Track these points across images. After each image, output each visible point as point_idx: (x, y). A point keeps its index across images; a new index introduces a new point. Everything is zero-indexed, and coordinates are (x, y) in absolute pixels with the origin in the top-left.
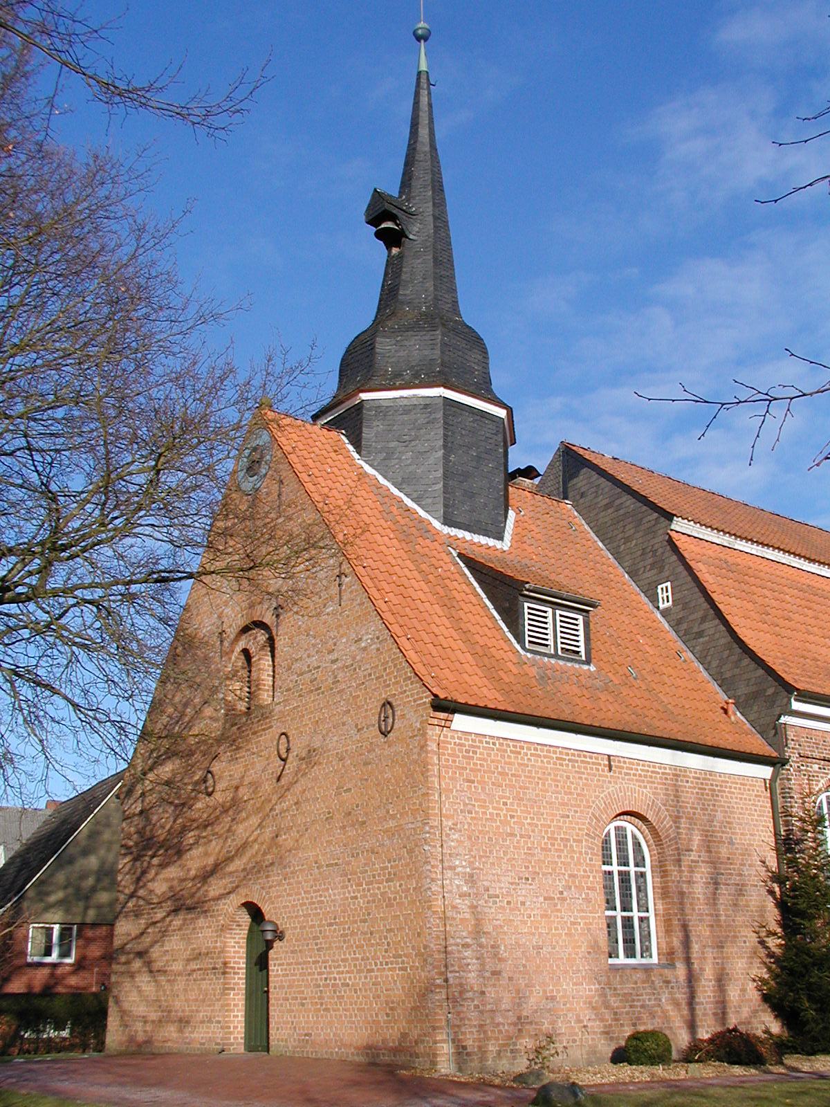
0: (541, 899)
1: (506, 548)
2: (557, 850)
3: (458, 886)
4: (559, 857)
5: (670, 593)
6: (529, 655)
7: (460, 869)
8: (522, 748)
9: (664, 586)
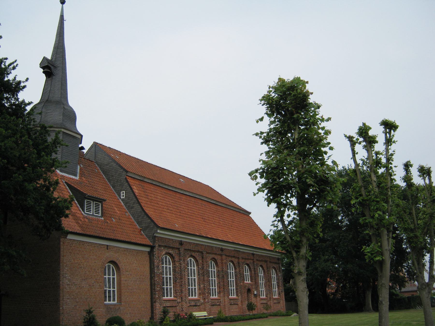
0: (88, 286)
1: (78, 179)
2: (92, 272)
3: (67, 282)
4: (93, 274)
5: (124, 194)
6: (86, 215)
7: (67, 278)
8: (85, 243)
9: (123, 192)
